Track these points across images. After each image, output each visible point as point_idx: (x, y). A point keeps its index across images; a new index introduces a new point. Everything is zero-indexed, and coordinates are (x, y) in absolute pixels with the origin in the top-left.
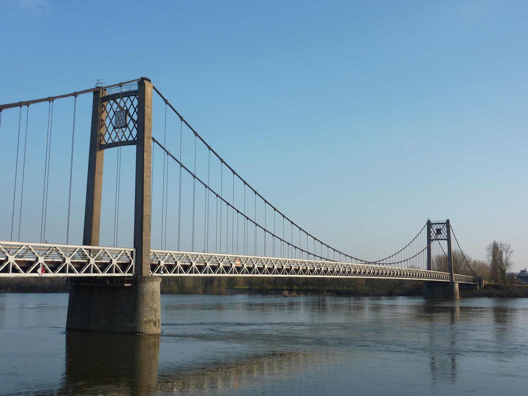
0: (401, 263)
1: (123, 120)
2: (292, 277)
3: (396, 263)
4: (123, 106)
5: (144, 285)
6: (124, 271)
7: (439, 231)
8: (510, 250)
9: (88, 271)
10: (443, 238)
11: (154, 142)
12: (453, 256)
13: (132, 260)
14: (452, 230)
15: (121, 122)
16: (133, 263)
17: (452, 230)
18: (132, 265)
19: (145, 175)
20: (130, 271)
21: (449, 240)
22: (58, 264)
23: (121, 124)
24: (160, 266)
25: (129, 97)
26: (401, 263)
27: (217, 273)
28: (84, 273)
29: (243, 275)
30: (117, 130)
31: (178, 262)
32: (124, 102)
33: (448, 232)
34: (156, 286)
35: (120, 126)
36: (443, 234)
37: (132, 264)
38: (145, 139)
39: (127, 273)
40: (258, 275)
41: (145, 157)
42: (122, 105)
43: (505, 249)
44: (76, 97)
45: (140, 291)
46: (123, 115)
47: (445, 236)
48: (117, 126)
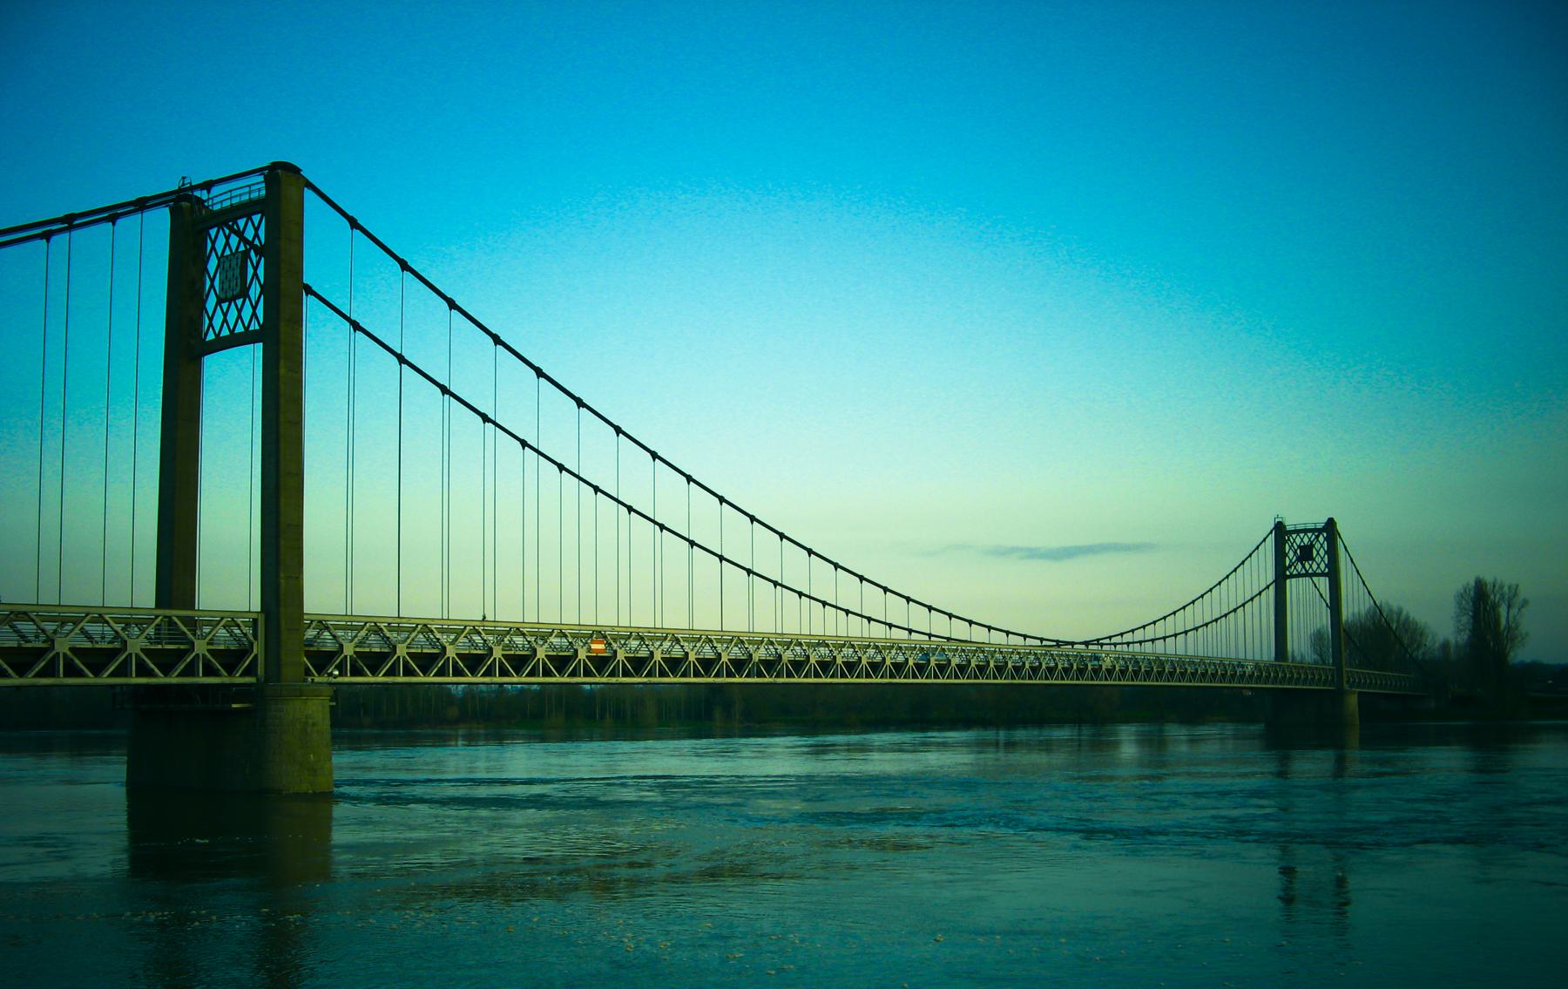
0: (484, 617)
2: (721, 684)
3: (1133, 643)
4: (251, 239)
6: (231, 670)
7: (1306, 553)
8: (1518, 601)
10: (1319, 571)
14: (1345, 548)
16: (258, 649)
17: (1345, 548)
18: (256, 656)
19: (282, 419)
21: (1333, 574)
22: (433, 658)
23: (233, 290)
24: (536, 659)
26: (484, 617)
27: (804, 677)
28: (383, 676)
29: (614, 680)
30: (225, 306)
31: (539, 649)
32: (226, 236)
33: (1332, 552)
34: (317, 710)
36: (1318, 559)
37: (255, 651)
38: (282, 324)
39: (568, 676)
40: (996, 681)
41: (282, 371)
42: (234, 240)
43: (1507, 597)
44: (48, 241)
46: (237, 264)
47: (1322, 566)
48: (223, 296)
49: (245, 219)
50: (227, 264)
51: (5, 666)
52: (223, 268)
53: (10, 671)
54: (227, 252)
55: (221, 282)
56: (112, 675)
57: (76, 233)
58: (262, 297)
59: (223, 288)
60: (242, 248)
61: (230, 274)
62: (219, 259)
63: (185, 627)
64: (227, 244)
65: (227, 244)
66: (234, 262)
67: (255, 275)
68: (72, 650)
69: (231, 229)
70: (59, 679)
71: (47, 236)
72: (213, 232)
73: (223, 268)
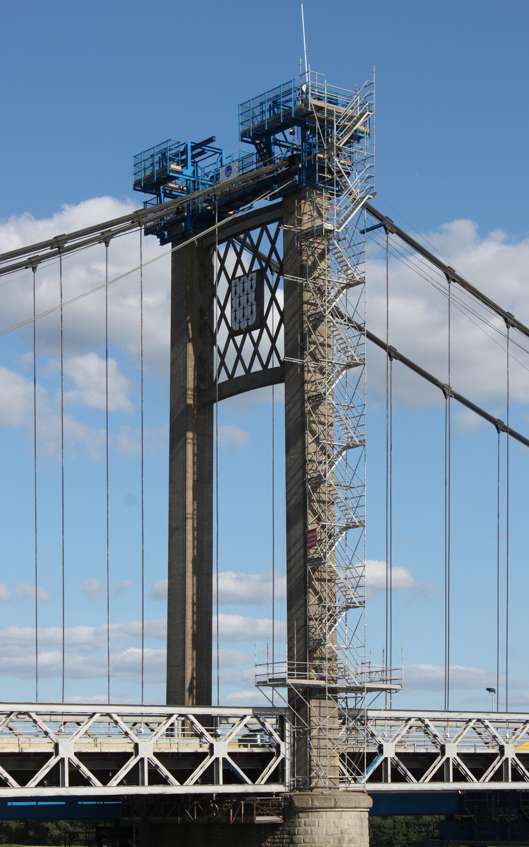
1: (252, 305)
4: (266, 254)
5: (313, 819)
9: (498, 777)
11: (511, 328)
12: (243, 737)
13: (282, 744)
15: (248, 311)
16: (285, 750)
20: (273, 779)
23: (248, 320)
25: (264, 227)
30: (239, 339)
35: (246, 326)
44: (34, 269)
45: (302, 837)
46: (252, 287)
48: (236, 328)
49: (259, 229)
50: (239, 289)
51: (6, 775)
52: (236, 293)
53: (11, 780)
54: (240, 273)
55: (234, 311)
56: (41, 784)
57: (67, 258)
58: (283, 326)
59: (235, 319)
60: (257, 266)
61: (244, 299)
62: (229, 281)
63: (203, 726)
64: (239, 262)
65: (239, 262)
66: (247, 286)
67: (273, 299)
68: (78, 755)
69: (244, 245)
70: (63, 789)
71: (33, 264)
72: (221, 248)
73: (236, 293)
